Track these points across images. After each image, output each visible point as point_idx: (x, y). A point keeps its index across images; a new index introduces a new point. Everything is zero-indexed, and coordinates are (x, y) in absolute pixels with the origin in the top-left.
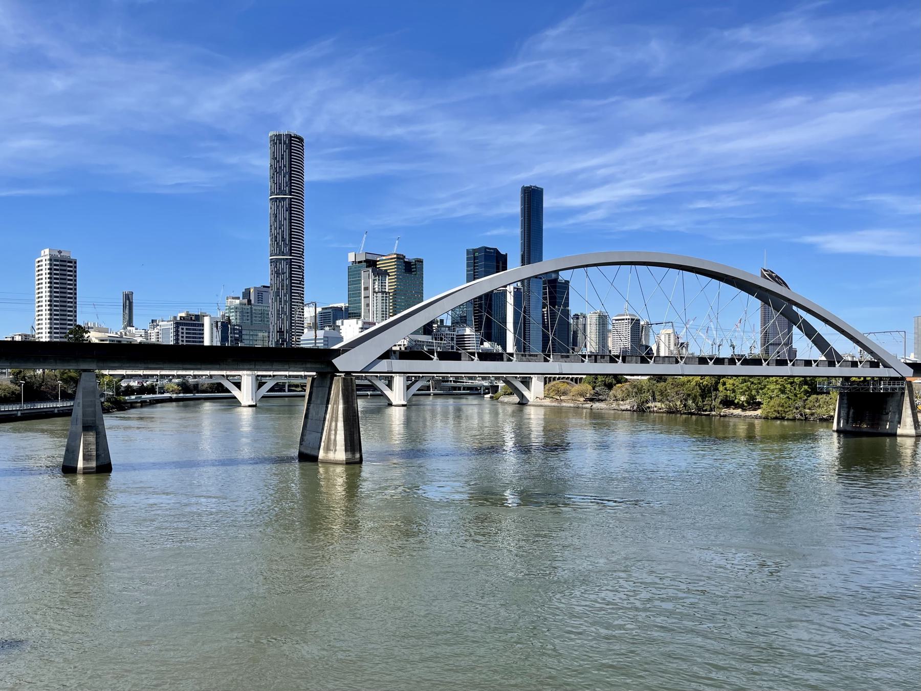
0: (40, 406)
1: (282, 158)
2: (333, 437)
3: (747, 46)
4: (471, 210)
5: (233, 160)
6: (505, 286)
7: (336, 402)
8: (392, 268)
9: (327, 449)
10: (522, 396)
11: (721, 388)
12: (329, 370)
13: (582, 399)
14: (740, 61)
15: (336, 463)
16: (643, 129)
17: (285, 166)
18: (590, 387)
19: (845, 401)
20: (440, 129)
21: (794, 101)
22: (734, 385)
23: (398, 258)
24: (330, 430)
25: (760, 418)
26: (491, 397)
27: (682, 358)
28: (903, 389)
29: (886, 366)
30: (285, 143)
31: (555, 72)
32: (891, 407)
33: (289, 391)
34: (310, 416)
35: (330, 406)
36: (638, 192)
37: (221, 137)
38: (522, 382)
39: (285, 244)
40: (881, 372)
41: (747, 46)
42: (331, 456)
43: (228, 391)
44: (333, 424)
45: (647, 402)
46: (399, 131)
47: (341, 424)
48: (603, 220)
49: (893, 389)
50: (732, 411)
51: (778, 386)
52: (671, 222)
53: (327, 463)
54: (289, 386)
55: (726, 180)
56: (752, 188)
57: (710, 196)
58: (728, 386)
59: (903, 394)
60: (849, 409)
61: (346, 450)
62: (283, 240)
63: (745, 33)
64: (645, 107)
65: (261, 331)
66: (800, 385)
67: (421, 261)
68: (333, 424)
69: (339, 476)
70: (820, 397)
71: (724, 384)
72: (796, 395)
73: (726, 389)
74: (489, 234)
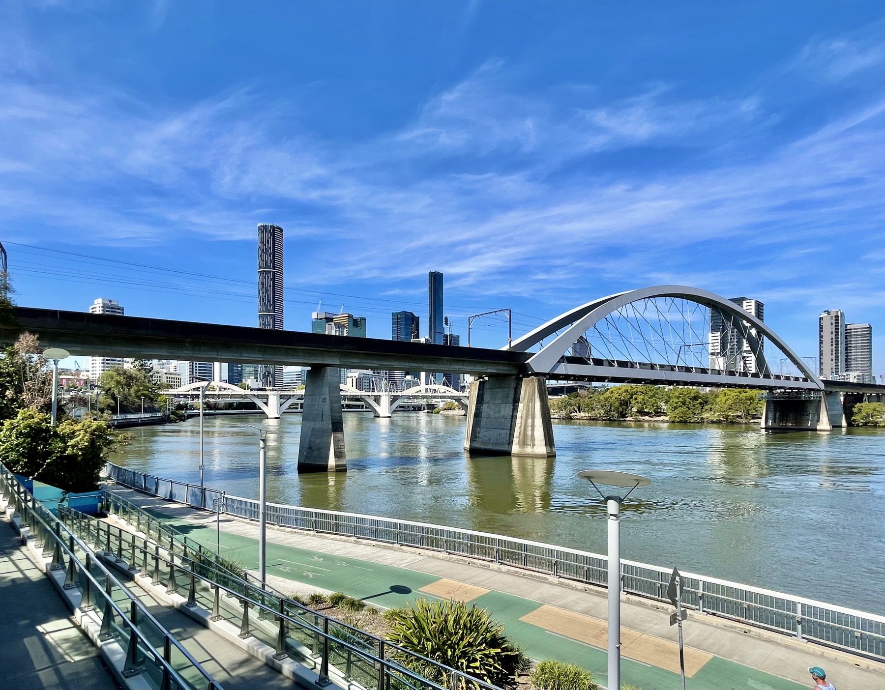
0: (130, 416)
2: (529, 433)
3: (600, 130)
4: (374, 273)
5: (173, 216)
14: (595, 143)
16: (506, 206)
20: (347, 193)
21: (619, 189)
25: (667, 422)
31: (450, 141)
32: (811, 410)
35: (521, 406)
36: (498, 263)
37: (158, 192)
39: (270, 305)
40: (809, 385)
41: (600, 130)
42: (529, 450)
43: (260, 409)
44: (530, 421)
46: (314, 195)
48: (471, 286)
51: (681, 399)
55: (562, 257)
56: (578, 264)
57: (548, 269)
59: (820, 401)
60: (775, 411)
63: (600, 117)
64: (512, 185)
67: (364, 319)
68: (530, 421)
69: (540, 467)
71: (636, 399)
74: (387, 293)
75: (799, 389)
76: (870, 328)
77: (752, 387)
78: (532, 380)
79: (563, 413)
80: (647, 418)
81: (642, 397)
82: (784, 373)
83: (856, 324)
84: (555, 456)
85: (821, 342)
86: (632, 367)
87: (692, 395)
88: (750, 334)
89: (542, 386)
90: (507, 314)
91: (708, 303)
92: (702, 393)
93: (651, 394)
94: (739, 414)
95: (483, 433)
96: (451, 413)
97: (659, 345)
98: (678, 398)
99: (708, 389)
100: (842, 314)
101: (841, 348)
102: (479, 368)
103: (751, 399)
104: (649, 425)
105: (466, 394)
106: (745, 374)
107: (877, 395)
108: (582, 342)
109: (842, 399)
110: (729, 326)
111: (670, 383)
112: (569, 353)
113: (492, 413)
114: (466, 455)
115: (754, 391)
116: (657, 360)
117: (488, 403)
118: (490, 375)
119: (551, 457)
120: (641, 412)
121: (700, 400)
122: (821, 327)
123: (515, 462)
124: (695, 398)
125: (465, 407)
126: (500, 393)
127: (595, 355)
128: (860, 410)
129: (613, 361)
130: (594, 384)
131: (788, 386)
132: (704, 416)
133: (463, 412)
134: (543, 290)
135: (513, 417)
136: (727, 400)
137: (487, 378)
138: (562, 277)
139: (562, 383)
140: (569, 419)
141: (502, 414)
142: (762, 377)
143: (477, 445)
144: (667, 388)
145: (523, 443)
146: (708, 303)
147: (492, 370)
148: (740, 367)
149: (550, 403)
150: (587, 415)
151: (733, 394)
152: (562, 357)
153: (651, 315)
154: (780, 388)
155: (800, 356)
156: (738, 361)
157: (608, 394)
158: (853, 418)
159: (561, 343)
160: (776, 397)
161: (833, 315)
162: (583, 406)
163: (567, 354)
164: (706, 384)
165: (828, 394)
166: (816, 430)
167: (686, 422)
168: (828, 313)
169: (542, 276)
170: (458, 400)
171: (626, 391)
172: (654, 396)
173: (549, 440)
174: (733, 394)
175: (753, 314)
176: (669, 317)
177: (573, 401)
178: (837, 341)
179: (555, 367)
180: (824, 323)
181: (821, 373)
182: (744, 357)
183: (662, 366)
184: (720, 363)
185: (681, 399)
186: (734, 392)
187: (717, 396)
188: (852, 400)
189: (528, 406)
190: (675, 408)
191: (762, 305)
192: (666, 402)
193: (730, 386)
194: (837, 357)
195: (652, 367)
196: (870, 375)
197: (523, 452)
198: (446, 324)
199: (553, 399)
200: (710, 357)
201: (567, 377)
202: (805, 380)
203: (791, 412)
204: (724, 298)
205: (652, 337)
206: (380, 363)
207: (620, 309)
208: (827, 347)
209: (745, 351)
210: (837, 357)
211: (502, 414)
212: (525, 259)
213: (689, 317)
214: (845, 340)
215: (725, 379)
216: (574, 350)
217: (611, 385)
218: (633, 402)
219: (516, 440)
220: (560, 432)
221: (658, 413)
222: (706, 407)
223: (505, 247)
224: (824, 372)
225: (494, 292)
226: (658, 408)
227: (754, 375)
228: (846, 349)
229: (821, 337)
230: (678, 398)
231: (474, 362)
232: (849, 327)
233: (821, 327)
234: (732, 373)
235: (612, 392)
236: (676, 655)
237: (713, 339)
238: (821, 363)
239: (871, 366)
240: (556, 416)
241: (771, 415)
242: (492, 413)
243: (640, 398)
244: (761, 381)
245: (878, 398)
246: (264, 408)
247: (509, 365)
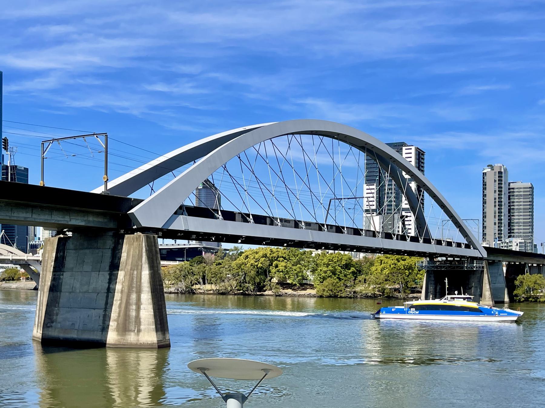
2: (133, 314)
7: (137, 267)
19: (433, 278)
22: (286, 267)
25: (314, 296)
28: (483, 267)
29: (475, 248)
35: (121, 275)
36: (96, 60)
42: (132, 338)
44: (134, 296)
48: (54, 91)
51: (330, 268)
52: (125, 104)
57: (170, 78)
61: (157, 330)
68: (134, 296)
69: (147, 362)
71: (277, 266)
73: (278, 271)
76: (532, 188)
77: (411, 254)
78: (138, 239)
79: (182, 285)
80: (289, 291)
81: (283, 264)
83: (520, 184)
85: (484, 202)
86: (272, 223)
87: (344, 262)
88: (409, 188)
89: (152, 248)
90: (101, 141)
91: (363, 147)
92: (355, 260)
93: (294, 260)
94: (397, 286)
95: (62, 315)
96: (13, 285)
97: (306, 197)
98: (328, 265)
99: (362, 255)
100: (505, 170)
101: (505, 210)
102: (59, 218)
103: (410, 268)
104: (293, 302)
105: (39, 256)
106: (403, 238)
107: (538, 265)
108: (209, 186)
109: (505, 269)
110: (387, 177)
111: (317, 246)
112: (191, 202)
113: (78, 285)
114: (36, 348)
115: (413, 258)
116: (303, 216)
117: (72, 270)
118: (73, 229)
119: (163, 347)
120: (283, 284)
121: (353, 269)
122: (484, 184)
123: (112, 358)
124: (347, 266)
125: (35, 276)
126: (89, 256)
127: (226, 206)
128: (522, 282)
129: (248, 215)
130: (225, 245)
131: (449, 253)
132: (358, 289)
133: (33, 284)
134: (161, 108)
135: (110, 292)
136: (383, 269)
137: (70, 234)
138: (190, 91)
139: (182, 243)
140: (190, 293)
141: (92, 287)
142: (421, 241)
143: (54, 333)
144: (315, 252)
145: (124, 329)
146: (363, 147)
147: (78, 221)
148: (398, 229)
149: (163, 271)
150: (214, 287)
151: (390, 262)
152: (181, 207)
153: (294, 154)
154: (442, 255)
155: (462, 218)
156: (396, 221)
157: (242, 259)
158: (515, 292)
159: (180, 188)
160: (437, 267)
161: (497, 170)
162: (209, 276)
163: (188, 203)
164: (360, 249)
165: (491, 264)
167: (336, 297)
168: (491, 167)
169: (160, 87)
170: (25, 265)
171: (265, 256)
172: (298, 263)
173: (161, 322)
174: (390, 262)
175: (413, 163)
176: (317, 159)
177: (196, 268)
178: (500, 202)
179: (171, 220)
180: (487, 179)
181: (484, 239)
182: (402, 217)
183: (308, 224)
184: (376, 223)
185: (330, 268)
186: (391, 260)
187: (372, 264)
188: (515, 271)
189: (131, 275)
190: (324, 279)
192: (313, 271)
193: (387, 251)
194: (500, 220)
195: (297, 224)
196: (532, 243)
197: (123, 342)
198: (6, 149)
199: (168, 266)
200: (365, 215)
201: (187, 235)
202: (467, 246)
204: (380, 142)
205: (297, 186)
207: (257, 147)
208: (491, 209)
209: (404, 209)
210: (500, 220)
211: (92, 287)
212: (140, 59)
213: (340, 161)
214: (508, 203)
215: (380, 242)
216: (199, 198)
217: (246, 247)
218: (273, 270)
219: (113, 324)
220: (179, 314)
221: (304, 285)
222: (361, 278)
223: (108, 36)
224: (487, 237)
225: (88, 104)
226: (304, 278)
227: (414, 239)
228: (509, 212)
229: (484, 195)
230: (328, 265)
231: (83, 212)
232: (512, 186)
233: (484, 184)
234: (388, 236)
235: (247, 257)
237: (369, 193)
238: (484, 227)
239: (532, 232)
240: (172, 290)
241: (431, 288)
242: (78, 285)
243: (282, 265)
244: (421, 247)
245: (539, 269)
247: (104, 215)
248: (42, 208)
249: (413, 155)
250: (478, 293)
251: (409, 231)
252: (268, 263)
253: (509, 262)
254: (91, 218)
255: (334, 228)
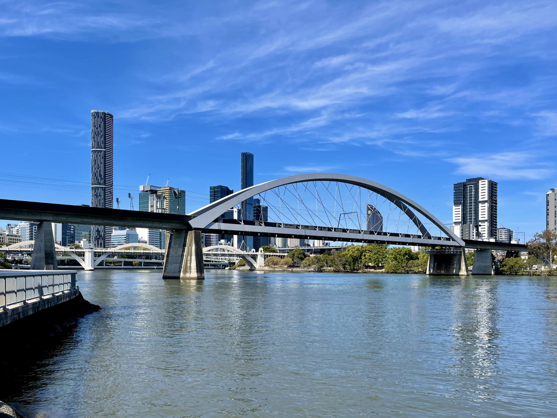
1: (100, 127)
2: (189, 265)
6: (232, 208)
7: (191, 245)
8: (167, 195)
9: (185, 272)
10: (251, 265)
11: (363, 258)
12: (184, 227)
13: (286, 266)
15: (191, 279)
17: (101, 131)
18: (291, 260)
19: (433, 259)
23: (170, 189)
24: (187, 261)
26: (229, 269)
27: (362, 231)
28: (461, 252)
29: (454, 240)
30: (101, 117)
33: (106, 265)
34: (170, 255)
38: (252, 257)
39: (101, 179)
40: (451, 243)
42: (188, 275)
44: (189, 257)
45: (323, 267)
47: (194, 257)
49: (457, 252)
50: (369, 270)
53: (185, 279)
54: (106, 263)
58: (367, 256)
60: (434, 263)
61: (197, 272)
62: (100, 175)
65: (85, 231)
66: (404, 256)
67: (184, 192)
68: (189, 257)
70: (414, 261)
71: (365, 256)
72: (402, 260)
75: (442, 246)
81: (368, 254)
82: (402, 230)
84: (204, 279)
85: (548, 214)
122: (548, 202)
135: (182, 255)
143: (166, 275)
156: (471, 229)
166: (458, 275)
191: (496, 184)
202: (448, 239)
203: (444, 261)
206: (82, 220)
229: (548, 210)
233: (548, 202)
236: (16, 300)
241: (432, 265)
246: (82, 263)
248: (96, 218)
249: (486, 186)
250: (458, 267)
251: (483, 235)
252: (359, 254)
253: (508, 251)
254: (173, 225)
255: (327, 229)
